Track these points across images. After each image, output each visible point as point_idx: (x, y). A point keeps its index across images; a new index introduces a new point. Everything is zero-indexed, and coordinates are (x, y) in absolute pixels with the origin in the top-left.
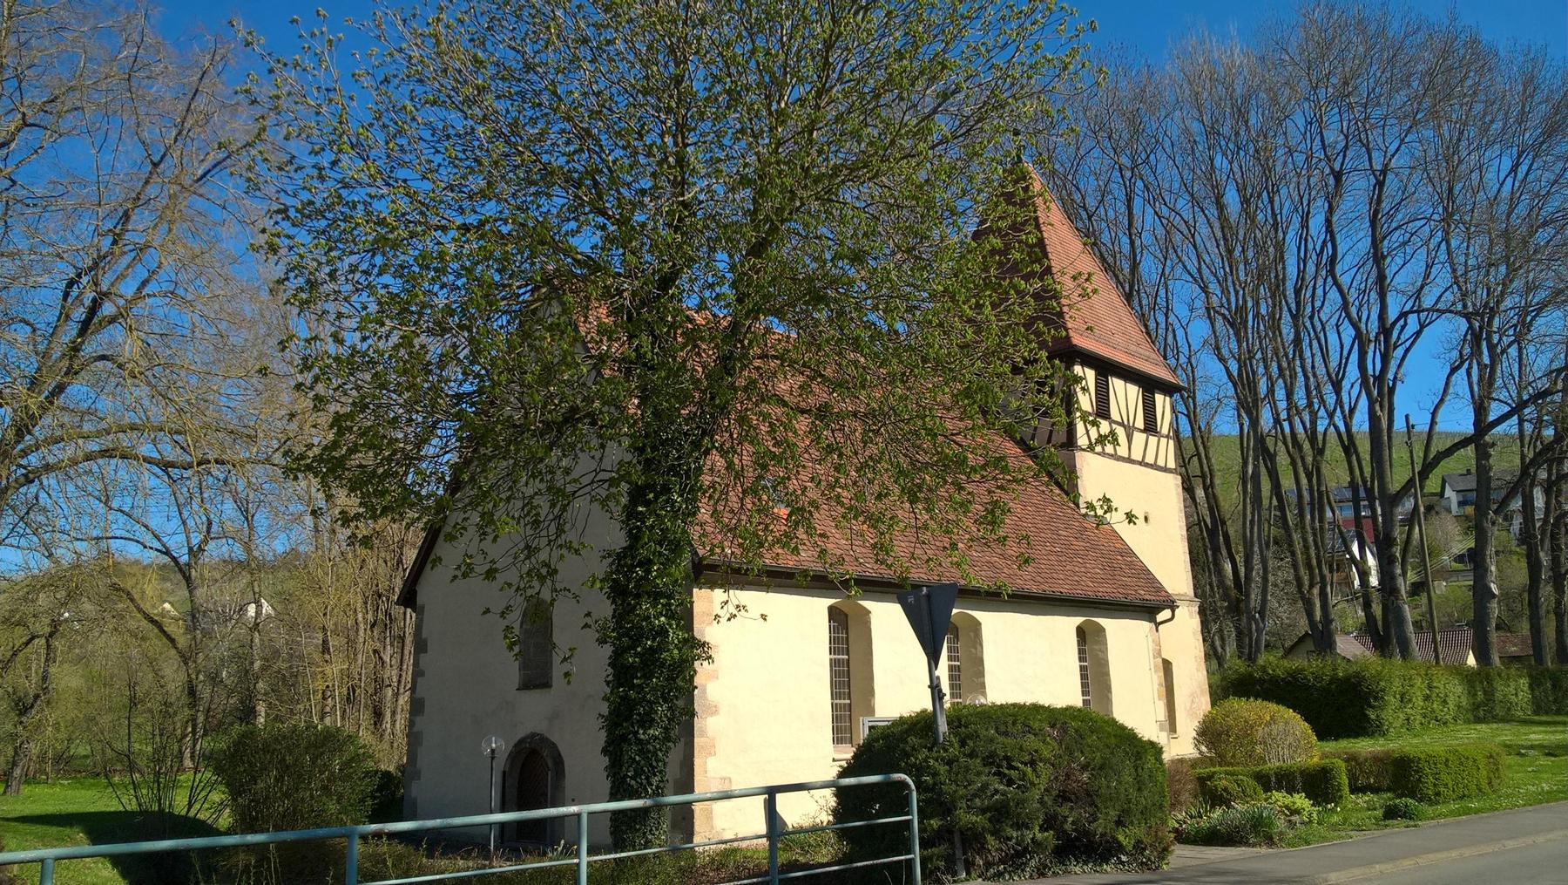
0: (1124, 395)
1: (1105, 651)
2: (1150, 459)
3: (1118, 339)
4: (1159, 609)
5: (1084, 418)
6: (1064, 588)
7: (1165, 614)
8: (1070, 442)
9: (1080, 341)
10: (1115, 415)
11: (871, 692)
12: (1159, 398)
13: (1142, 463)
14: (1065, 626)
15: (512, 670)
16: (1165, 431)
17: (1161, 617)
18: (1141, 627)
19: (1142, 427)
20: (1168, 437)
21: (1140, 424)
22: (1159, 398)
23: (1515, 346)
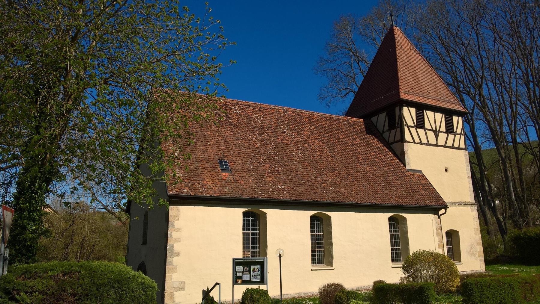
0: (434, 119)
1: (406, 228)
2: (456, 145)
3: (432, 95)
4: (440, 209)
5: (409, 127)
6: (378, 201)
7: (442, 211)
8: (402, 140)
9: (404, 96)
10: (427, 126)
11: (266, 246)
12: (455, 118)
13: (445, 146)
14: (383, 218)
15: (141, 242)
16: (459, 131)
17: (441, 212)
18: (430, 217)
19: (445, 131)
20: (461, 134)
21: (443, 129)
22: (455, 118)
23: (385, 130)
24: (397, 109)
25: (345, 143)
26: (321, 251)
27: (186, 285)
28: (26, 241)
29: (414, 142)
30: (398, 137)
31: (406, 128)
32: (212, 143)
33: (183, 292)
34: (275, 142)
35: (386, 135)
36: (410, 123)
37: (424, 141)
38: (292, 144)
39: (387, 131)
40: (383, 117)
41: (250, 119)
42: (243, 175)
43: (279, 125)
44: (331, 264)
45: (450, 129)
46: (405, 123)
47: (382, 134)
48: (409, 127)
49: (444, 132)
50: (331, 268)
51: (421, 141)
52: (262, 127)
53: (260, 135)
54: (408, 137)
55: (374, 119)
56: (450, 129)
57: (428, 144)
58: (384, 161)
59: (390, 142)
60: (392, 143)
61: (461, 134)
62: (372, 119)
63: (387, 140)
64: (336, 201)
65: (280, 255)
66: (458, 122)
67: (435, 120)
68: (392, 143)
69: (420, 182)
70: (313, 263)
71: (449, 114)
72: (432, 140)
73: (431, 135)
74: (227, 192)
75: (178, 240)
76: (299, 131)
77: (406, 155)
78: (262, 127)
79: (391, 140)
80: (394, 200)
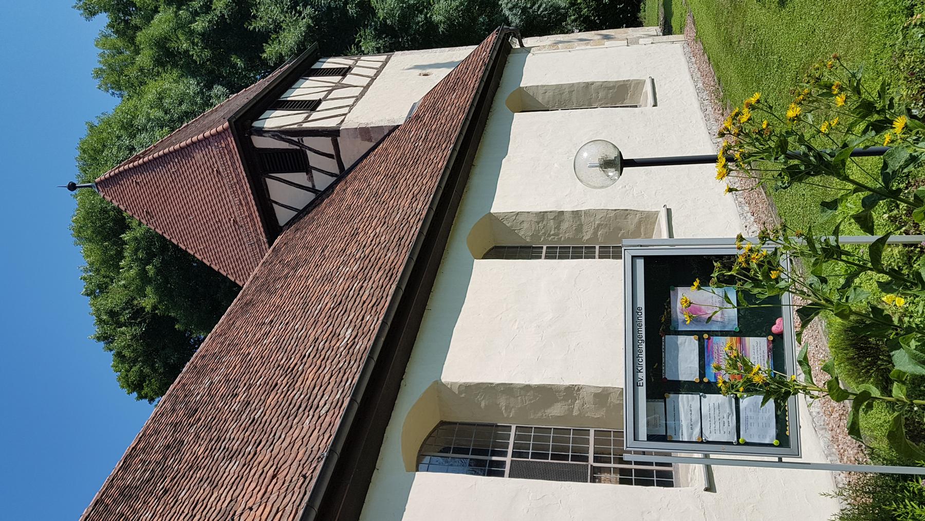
8: (333, 134)
24: (260, 142)
29: (345, 114)
30: (325, 144)
31: (305, 125)
35: (322, 182)
39: (311, 178)
48: (306, 120)
50: (648, 87)
54: (331, 123)
59: (336, 171)
65: (607, 164)
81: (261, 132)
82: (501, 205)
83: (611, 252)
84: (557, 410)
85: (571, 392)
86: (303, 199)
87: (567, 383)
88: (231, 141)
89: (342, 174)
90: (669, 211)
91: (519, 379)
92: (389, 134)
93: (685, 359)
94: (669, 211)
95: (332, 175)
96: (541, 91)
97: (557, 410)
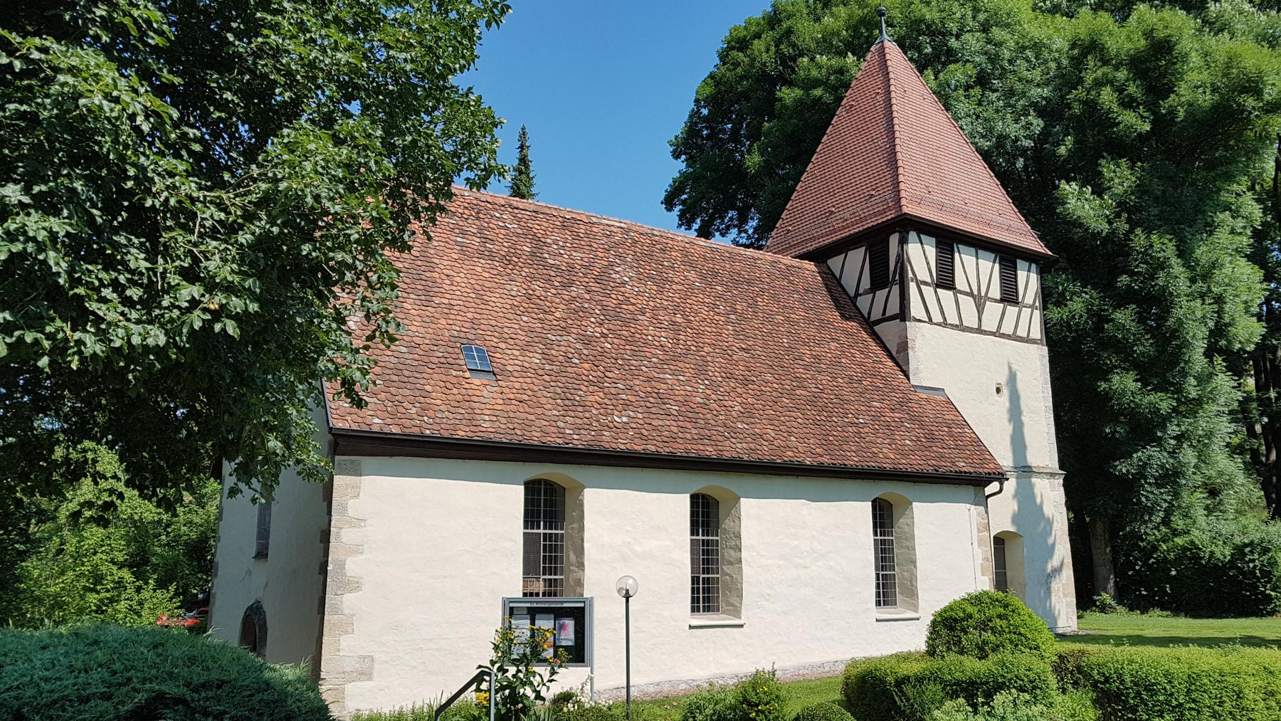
0: (975, 269)
2: (1022, 332)
7: (993, 487)
8: (903, 315)
10: (960, 283)
13: (997, 334)
16: (1029, 299)
19: (998, 297)
21: (995, 292)
23: (861, 291)
24: (894, 240)
25: (769, 318)
26: (710, 588)
27: (377, 667)
28: (1108, 321)
30: (894, 308)
31: (913, 286)
32: (446, 301)
33: (367, 684)
34: (604, 308)
35: (863, 303)
36: (923, 275)
37: (952, 319)
38: (644, 314)
39: (866, 292)
40: (857, 257)
41: (539, 243)
42: (525, 386)
43: (611, 265)
44: (736, 612)
45: (1009, 296)
46: (910, 275)
47: (853, 300)
49: (996, 301)
51: (945, 319)
52: (571, 267)
53: (566, 285)
54: (916, 309)
55: (835, 263)
56: (1009, 296)
57: (960, 327)
58: (861, 365)
59: (872, 319)
60: (878, 322)
61: (1032, 307)
62: (830, 262)
63: (865, 313)
64: (754, 457)
66: (1028, 281)
67: (978, 269)
68: (878, 322)
69: (944, 421)
70: (695, 609)
71: (1008, 256)
72: (970, 319)
73: (968, 304)
74: (489, 428)
75: (357, 550)
76: (662, 282)
77: (910, 351)
78: (571, 267)
79: (876, 314)
80: (886, 457)
81: (903, 241)
82: (746, 504)
83: (1001, 581)
84: (573, 557)
85: (581, 566)
86: (849, 283)
87: (586, 563)
88: (890, 215)
89: (869, 325)
90: (742, 626)
91: (587, 536)
92: (902, 371)
93: (545, 624)
94: (742, 626)
95: (869, 313)
96: (909, 521)
97: (573, 557)
